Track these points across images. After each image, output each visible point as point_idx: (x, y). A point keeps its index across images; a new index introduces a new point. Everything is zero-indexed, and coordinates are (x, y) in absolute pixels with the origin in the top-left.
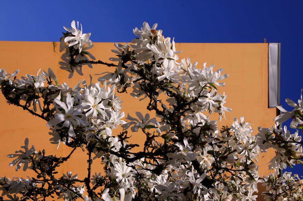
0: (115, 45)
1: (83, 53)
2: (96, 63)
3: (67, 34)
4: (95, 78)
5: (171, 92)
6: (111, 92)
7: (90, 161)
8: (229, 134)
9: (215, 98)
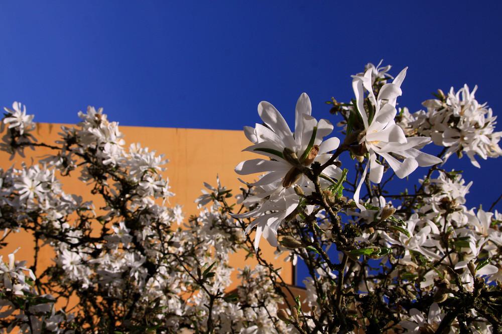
0: (62, 128)
1: (25, 135)
2: (39, 145)
3: (9, 115)
4: (36, 160)
5: (116, 176)
6: (51, 175)
7: (37, 249)
8: (197, 224)
9: (158, 183)
